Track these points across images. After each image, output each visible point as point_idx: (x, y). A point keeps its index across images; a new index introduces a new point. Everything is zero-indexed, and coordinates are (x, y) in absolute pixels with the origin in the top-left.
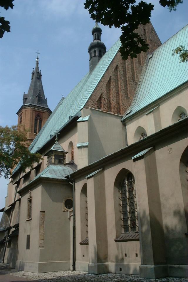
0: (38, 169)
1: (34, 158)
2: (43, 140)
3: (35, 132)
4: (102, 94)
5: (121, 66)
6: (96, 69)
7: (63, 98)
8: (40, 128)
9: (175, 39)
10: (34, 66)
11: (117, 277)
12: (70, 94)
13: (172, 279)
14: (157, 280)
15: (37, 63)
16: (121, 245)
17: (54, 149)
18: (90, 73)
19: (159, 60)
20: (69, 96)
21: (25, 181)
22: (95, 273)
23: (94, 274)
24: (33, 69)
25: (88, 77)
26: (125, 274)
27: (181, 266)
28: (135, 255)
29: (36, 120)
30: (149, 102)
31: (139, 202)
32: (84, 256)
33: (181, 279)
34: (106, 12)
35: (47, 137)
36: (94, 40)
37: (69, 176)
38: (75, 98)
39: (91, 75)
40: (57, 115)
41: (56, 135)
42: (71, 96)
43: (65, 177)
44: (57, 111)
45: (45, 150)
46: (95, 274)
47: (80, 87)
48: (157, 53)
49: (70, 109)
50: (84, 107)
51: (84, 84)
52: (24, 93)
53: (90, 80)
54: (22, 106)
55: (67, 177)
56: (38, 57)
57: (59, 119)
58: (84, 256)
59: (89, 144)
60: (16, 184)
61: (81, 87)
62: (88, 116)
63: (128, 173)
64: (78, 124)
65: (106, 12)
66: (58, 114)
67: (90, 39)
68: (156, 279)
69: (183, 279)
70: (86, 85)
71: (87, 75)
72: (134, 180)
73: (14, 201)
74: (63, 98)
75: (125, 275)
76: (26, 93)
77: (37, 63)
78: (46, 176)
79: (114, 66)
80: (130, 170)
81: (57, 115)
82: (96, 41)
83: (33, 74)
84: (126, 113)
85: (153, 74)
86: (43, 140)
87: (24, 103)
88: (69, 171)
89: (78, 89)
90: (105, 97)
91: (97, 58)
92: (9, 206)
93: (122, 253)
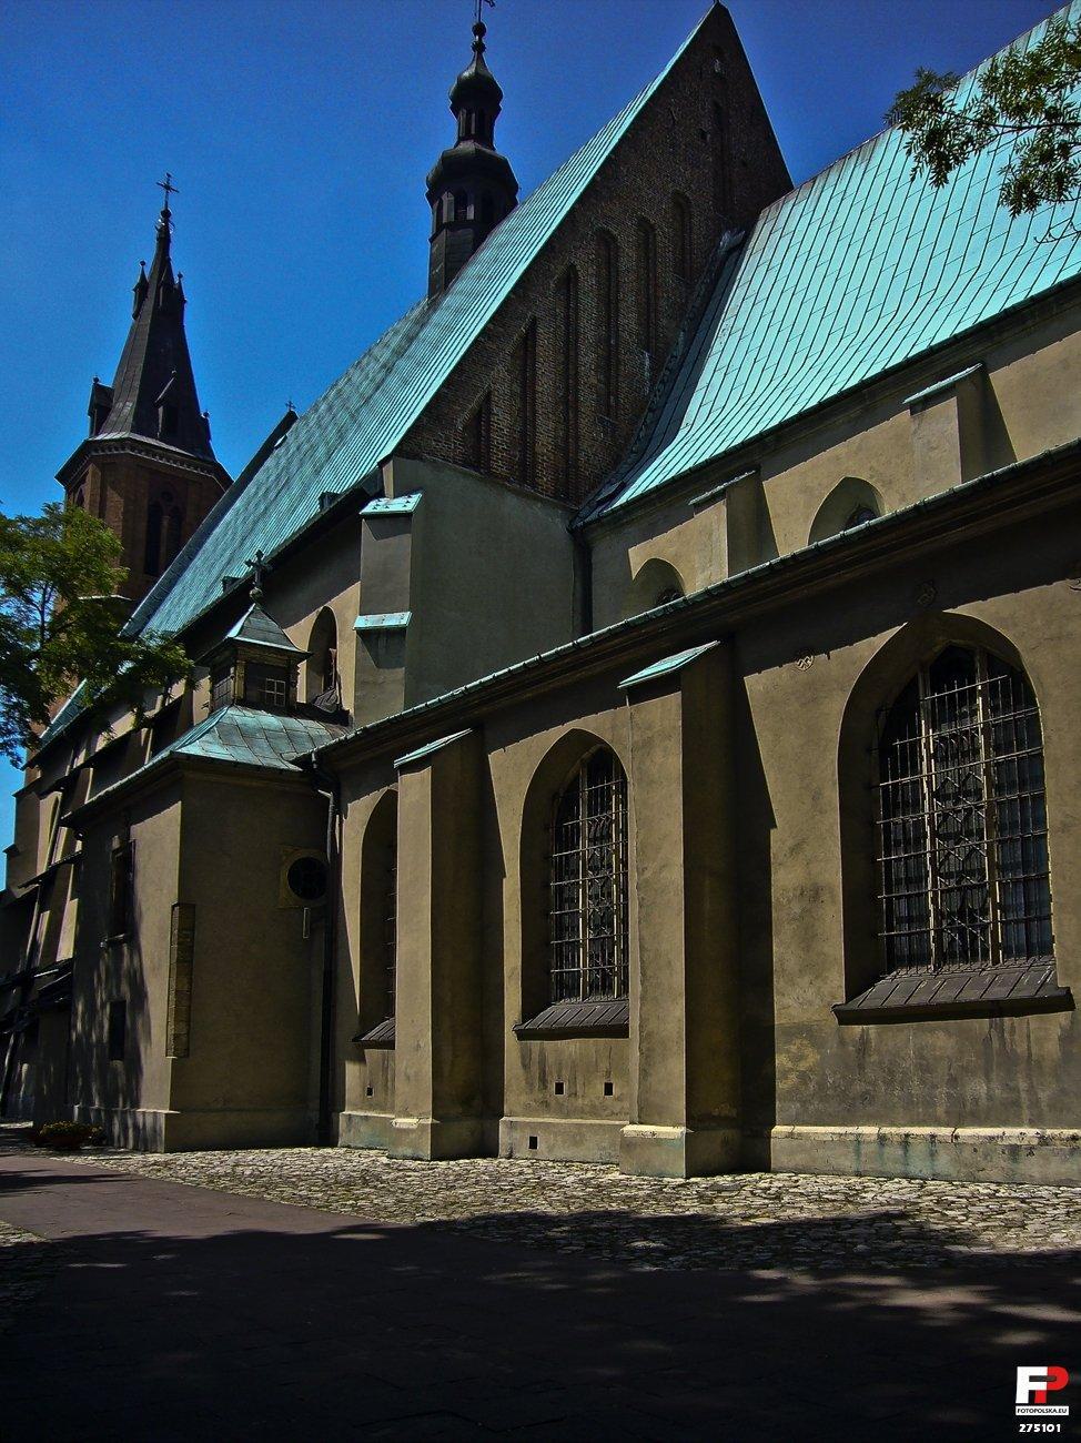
0: (174, 722)
1: (158, 669)
2: (187, 604)
3: (153, 570)
4: (490, 393)
5: (591, 271)
6: (462, 285)
7: (291, 419)
8: (178, 543)
9: (863, 165)
10: (150, 255)
11: (517, 1170)
12: (326, 398)
13: (756, 1176)
14: (693, 1180)
15: (164, 240)
16: (1013, 1027)
17: (244, 636)
18: (433, 305)
19: (777, 261)
20: (323, 407)
21: (99, 782)
22: (421, 1154)
23: (416, 1160)
24: (143, 263)
25: (422, 322)
26: (553, 1161)
27: (799, 1129)
28: (602, 1088)
29: (154, 514)
30: (680, 465)
31: (641, 871)
32: (370, 1092)
33: (795, 1178)
34: (26, 705)
35: (208, 592)
36: (461, 139)
37: (314, 759)
38: (352, 416)
39: (435, 311)
40: (256, 493)
41: (252, 579)
42: (330, 408)
43: (292, 762)
44: (259, 476)
45: (205, 632)
46: (421, 1160)
47: (377, 367)
48: (768, 227)
49: (322, 467)
50: (398, 451)
51: (399, 353)
52: (96, 380)
53: (429, 332)
54: (87, 447)
55: (302, 761)
56: (495, 68)
57: (266, 509)
58: (370, 1092)
59: (412, 620)
60: (59, 794)
61: (384, 366)
62: (415, 498)
63: (593, 750)
64: (365, 528)
65: (26, 705)
66: (264, 489)
67: (445, 135)
68: (687, 1178)
69: (805, 1178)
70: (436, 325)
71: (417, 312)
72: (623, 788)
73: (49, 863)
74: (291, 419)
75: (550, 1164)
76: (108, 382)
77: (164, 240)
78: (201, 753)
79: (559, 270)
80: (607, 738)
81: (256, 493)
82: (469, 147)
83: (142, 289)
84: (598, 494)
85: (740, 323)
86: (187, 604)
87: (96, 429)
88: (316, 736)
89: (367, 377)
90: (503, 419)
91: (468, 234)
92: (26, 886)
93: (543, 1081)
